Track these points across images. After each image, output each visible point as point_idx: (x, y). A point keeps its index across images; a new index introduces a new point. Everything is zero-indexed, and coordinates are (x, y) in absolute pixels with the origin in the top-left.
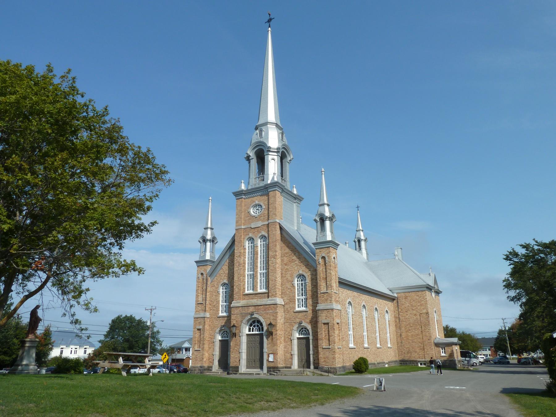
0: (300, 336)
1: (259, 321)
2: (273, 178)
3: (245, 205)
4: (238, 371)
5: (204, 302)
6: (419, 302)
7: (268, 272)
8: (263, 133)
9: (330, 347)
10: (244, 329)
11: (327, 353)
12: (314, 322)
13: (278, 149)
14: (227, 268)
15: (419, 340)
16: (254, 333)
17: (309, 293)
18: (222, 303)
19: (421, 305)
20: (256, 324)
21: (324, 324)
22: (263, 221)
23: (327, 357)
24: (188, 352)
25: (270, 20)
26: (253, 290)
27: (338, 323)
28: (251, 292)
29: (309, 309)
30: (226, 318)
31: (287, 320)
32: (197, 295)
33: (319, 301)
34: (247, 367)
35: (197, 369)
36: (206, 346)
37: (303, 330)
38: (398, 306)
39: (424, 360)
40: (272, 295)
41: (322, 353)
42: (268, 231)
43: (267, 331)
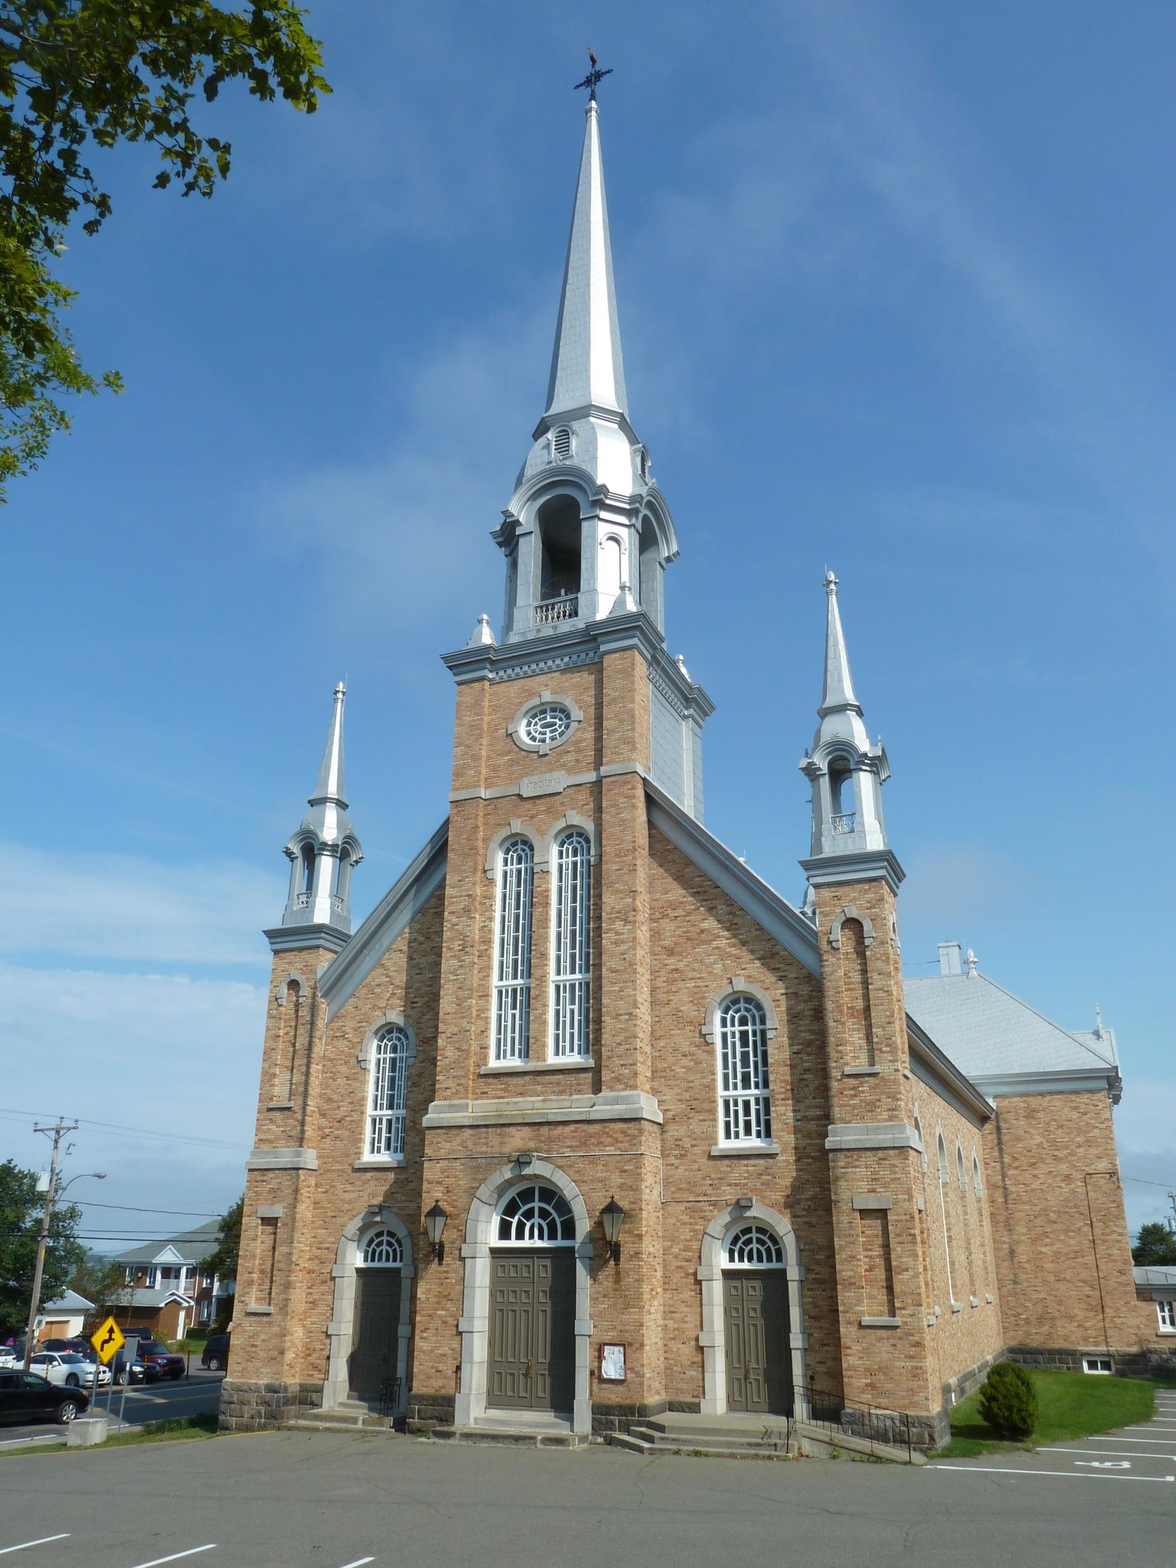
0: (737, 1265)
1: (550, 1194)
2: (620, 602)
3: (495, 709)
4: (447, 1417)
5: (296, 1104)
6: (1080, 1131)
7: (598, 979)
8: (574, 442)
9: (897, 1321)
10: (481, 1226)
11: (883, 1351)
12: (814, 1198)
13: (633, 499)
14: (402, 960)
15: (1085, 1275)
16: (526, 1243)
17: (780, 1076)
18: (373, 1109)
19: (1089, 1143)
20: (537, 1204)
21: (864, 1213)
22: (571, 771)
23: (884, 1370)
24: (173, 1281)
25: (593, 79)
26: (526, 1054)
27: (920, 1211)
28: (514, 1062)
29: (784, 1142)
30: (391, 1176)
31: (674, 1191)
32: (265, 1072)
33: (837, 1112)
34: (494, 1400)
35: (253, 1398)
36: (298, 1297)
37: (749, 1237)
38: (1000, 1143)
39: (1103, 1348)
40: (618, 1080)
41: (856, 1348)
42: (599, 809)
43: (591, 1238)
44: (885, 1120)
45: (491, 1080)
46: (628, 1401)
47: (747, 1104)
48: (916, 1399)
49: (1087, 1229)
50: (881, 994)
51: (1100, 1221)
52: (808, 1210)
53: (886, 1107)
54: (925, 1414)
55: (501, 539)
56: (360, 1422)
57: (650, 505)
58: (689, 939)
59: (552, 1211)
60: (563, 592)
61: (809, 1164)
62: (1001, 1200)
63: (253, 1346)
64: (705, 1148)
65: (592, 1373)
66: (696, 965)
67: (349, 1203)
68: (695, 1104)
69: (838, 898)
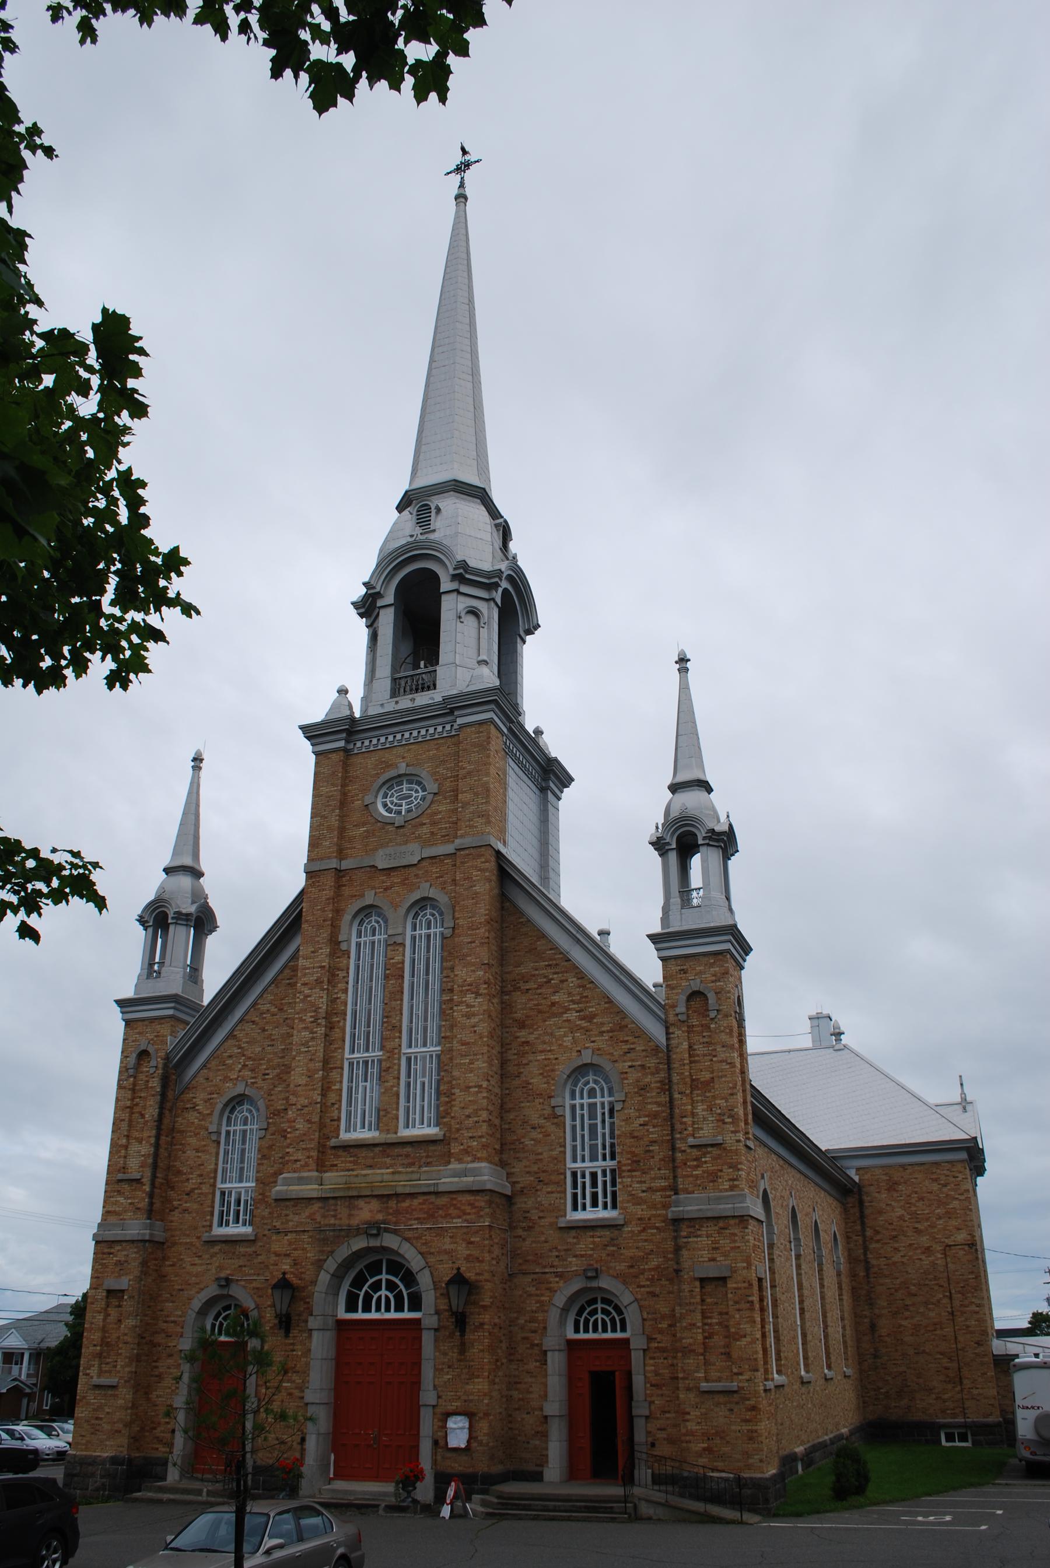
1: (397, 1267)
19: (949, 1215)
20: (384, 1277)
40: (466, 1152)
41: (695, 1413)
44: (726, 1190)
45: (340, 1153)
46: (471, 1470)
47: (594, 1175)
48: (751, 1461)
49: (946, 1301)
50: (725, 1066)
51: (959, 1292)
52: (652, 1280)
53: (726, 1178)
54: (759, 1475)
55: (362, 610)
56: (204, 1494)
57: (510, 578)
58: (540, 1012)
59: (399, 1283)
60: (422, 663)
61: (653, 1234)
62: (862, 1274)
63: (97, 1418)
64: (552, 1220)
65: (436, 1443)
66: (547, 1038)
67: (197, 1275)
68: (543, 1176)
69: (685, 972)
